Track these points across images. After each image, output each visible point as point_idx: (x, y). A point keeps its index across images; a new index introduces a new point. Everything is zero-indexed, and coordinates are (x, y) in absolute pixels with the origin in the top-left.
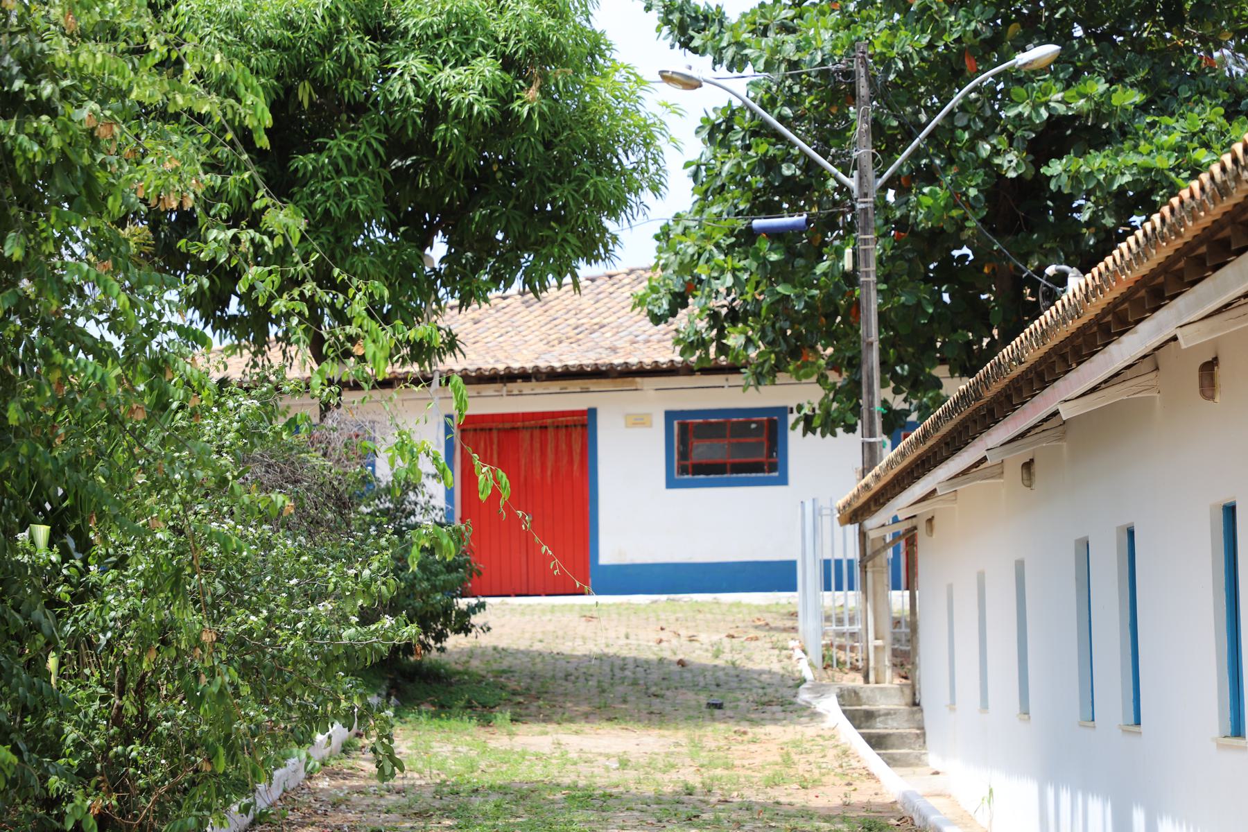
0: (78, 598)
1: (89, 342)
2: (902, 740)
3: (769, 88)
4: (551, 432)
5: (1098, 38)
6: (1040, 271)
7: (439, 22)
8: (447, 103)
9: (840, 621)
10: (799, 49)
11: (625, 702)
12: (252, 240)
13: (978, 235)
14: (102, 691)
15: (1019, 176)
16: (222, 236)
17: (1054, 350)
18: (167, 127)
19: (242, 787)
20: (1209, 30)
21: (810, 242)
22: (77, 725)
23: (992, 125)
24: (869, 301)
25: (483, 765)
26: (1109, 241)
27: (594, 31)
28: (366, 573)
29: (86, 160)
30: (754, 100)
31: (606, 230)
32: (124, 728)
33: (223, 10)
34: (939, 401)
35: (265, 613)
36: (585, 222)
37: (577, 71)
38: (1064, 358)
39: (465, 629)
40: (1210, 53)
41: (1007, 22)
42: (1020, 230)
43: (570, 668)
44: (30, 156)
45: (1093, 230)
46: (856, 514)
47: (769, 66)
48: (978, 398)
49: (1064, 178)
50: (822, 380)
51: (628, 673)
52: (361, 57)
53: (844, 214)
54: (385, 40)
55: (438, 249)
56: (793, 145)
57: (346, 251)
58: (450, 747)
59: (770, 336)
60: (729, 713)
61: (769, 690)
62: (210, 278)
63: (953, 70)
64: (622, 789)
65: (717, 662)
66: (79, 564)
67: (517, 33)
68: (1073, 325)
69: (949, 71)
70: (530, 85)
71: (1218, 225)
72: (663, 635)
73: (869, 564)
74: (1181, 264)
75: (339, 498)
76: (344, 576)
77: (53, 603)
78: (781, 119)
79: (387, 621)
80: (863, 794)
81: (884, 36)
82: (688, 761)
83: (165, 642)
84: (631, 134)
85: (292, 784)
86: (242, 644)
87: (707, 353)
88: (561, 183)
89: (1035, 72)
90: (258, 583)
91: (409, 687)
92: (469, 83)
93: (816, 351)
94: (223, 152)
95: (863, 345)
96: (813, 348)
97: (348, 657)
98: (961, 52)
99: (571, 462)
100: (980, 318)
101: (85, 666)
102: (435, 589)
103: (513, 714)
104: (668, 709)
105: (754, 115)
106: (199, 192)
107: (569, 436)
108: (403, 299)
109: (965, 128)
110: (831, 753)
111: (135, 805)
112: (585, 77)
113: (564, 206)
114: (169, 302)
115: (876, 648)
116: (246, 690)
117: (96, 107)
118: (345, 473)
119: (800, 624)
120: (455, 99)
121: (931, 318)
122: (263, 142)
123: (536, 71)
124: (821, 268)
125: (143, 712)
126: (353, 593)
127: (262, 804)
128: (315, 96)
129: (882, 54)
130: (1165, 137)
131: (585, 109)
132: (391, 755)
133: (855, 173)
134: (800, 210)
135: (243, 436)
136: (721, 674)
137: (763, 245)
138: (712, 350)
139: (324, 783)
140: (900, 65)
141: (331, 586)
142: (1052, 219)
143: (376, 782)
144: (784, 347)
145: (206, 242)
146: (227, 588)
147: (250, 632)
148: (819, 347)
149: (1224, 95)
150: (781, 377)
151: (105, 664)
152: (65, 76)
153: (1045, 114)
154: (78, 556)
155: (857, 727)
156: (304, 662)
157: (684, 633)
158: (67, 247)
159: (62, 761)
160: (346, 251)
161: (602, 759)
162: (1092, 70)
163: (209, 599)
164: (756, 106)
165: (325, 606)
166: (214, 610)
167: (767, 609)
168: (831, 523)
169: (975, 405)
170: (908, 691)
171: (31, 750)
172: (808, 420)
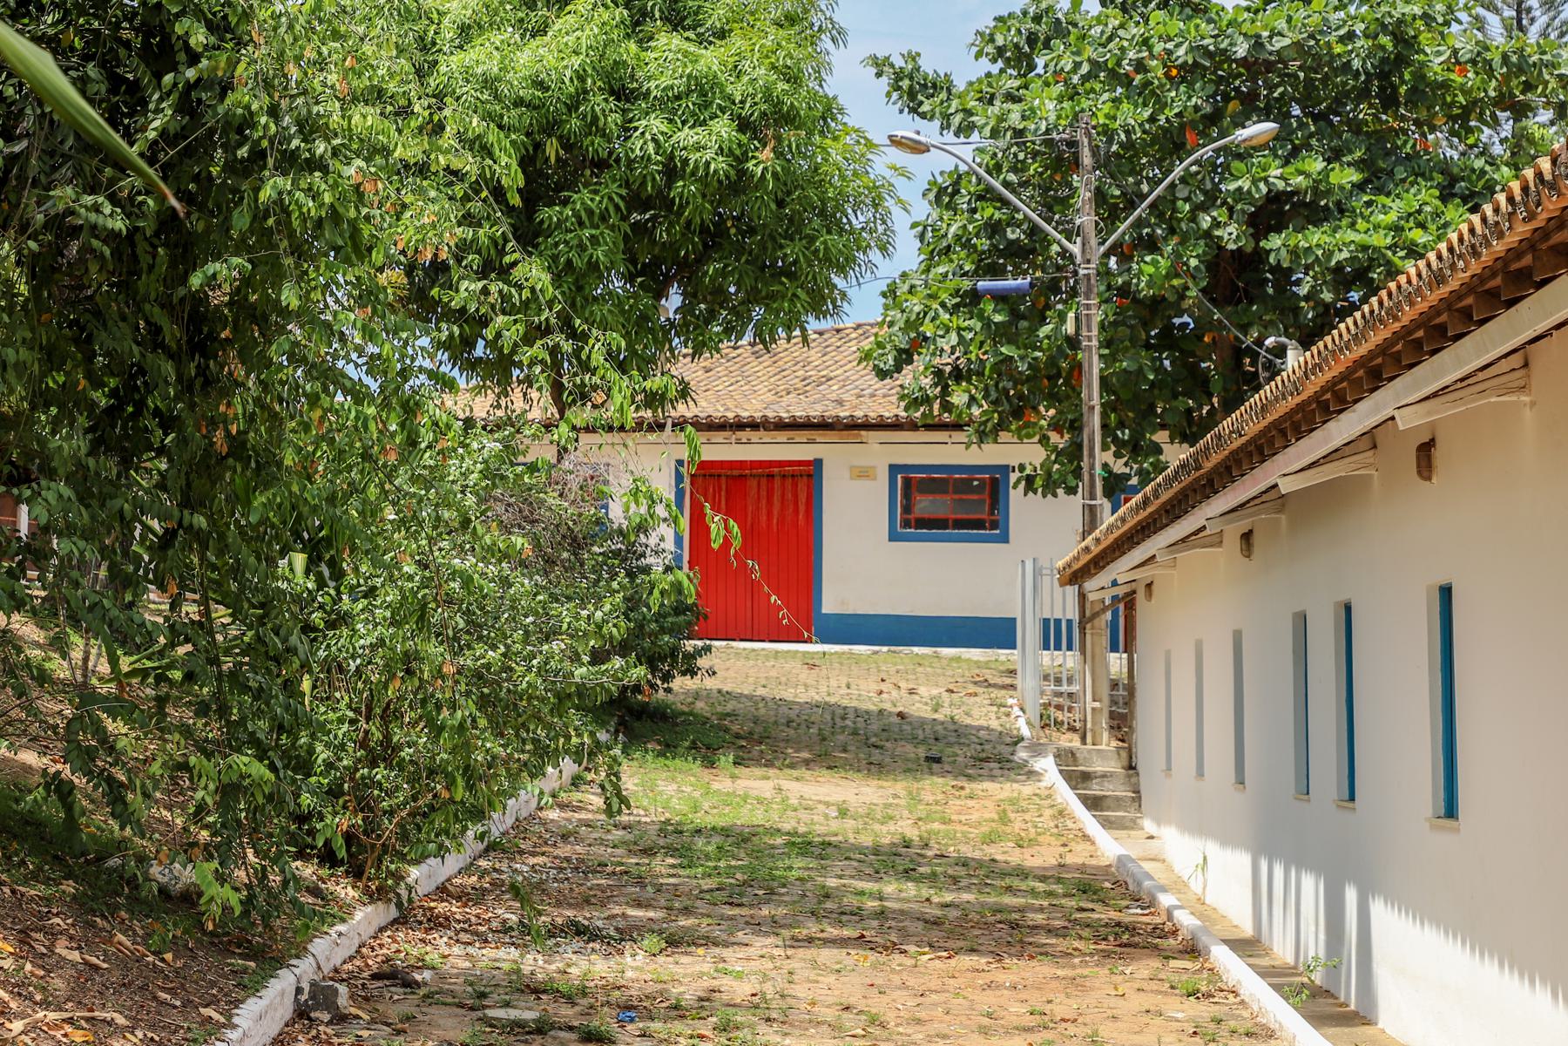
0: (331, 625)
1: (348, 384)
2: (1118, 802)
3: (995, 154)
4: (777, 482)
5: (1316, 118)
6: (1259, 342)
7: (680, 84)
8: (685, 162)
9: (1058, 681)
10: (1024, 118)
11: (845, 751)
12: (500, 291)
13: (1200, 305)
14: (351, 714)
15: (1239, 249)
16: (472, 287)
17: (1274, 424)
18: (425, 183)
19: (478, 814)
20: (1423, 115)
21: (1033, 304)
22: (327, 745)
23: (1211, 198)
24: (1091, 366)
25: (706, 806)
26: (1327, 318)
27: (826, 96)
28: (599, 614)
29: (352, 213)
30: (980, 165)
31: (835, 286)
32: (371, 751)
33: (479, 71)
34: (1159, 468)
35: (502, 649)
36: (814, 278)
37: (810, 134)
38: (1283, 433)
39: (691, 672)
40: (1423, 135)
41: (1227, 98)
42: (1240, 301)
43: (793, 715)
44: (305, 210)
45: (1312, 304)
46: (1076, 576)
47: (995, 134)
48: (1198, 468)
49: (1283, 252)
50: (1044, 441)
51: (848, 722)
52: (605, 117)
53: (1067, 279)
54: (628, 100)
56: (1018, 210)
57: (586, 300)
58: (675, 786)
59: (994, 395)
60: (947, 767)
61: (986, 747)
62: (460, 326)
63: (1174, 143)
64: (840, 838)
65: (936, 716)
66: (332, 592)
67: (754, 96)
68: (1292, 402)
69: (1171, 143)
70: (765, 146)
71: (1435, 311)
72: (883, 687)
73: (1088, 626)
74: (1399, 347)
75: (574, 539)
76: (577, 617)
77: (308, 628)
78: (1006, 184)
79: (617, 662)
80: (1078, 855)
81: (1106, 108)
82: (906, 813)
83: (409, 672)
84: (860, 194)
85: (524, 814)
86: (480, 677)
87: (931, 410)
88: (792, 240)
89: (1254, 148)
90: (497, 618)
91: (636, 724)
92: (708, 143)
93: (1038, 412)
94: (475, 206)
95: (1085, 409)
96: (1035, 409)
97: (580, 695)
98: (1182, 126)
99: (796, 511)
100: (1200, 385)
101: (336, 689)
102: (663, 630)
103: (736, 757)
104: (888, 760)
105: (979, 180)
106: (452, 244)
107: (795, 485)
108: (639, 347)
109: (1186, 200)
110: (1048, 813)
111: (379, 825)
112: (817, 139)
113: (795, 262)
114: (422, 349)
115: (1093, 709)
116: (483, 723)
117: (363, 164)
118: (580, 515)
119: (1018, 682)
120: (693, 157)
121: (1152, 384)
122: (515, 200)
123: (770, 133)
124: (1045, 330)
125: (387, 736)
126: (585, 634)
127: (495, 833)
128: (562, 152)
129: (1105, 125)
130: (1382, 216)
131: (816, 169)
132: (618, 794)
133: (1079, 240)
134: (1025, 273)
135: (486, 478)
136: (939, 728)
137: (988, 307)
138: (936, 406)
139: (554, 814)
140: (1123, 136)
141: (565, 626)
142: (1270, 291)
143: (603, 817)
144: (1006, 406)
145: (457, 291)
146: (467, 622)
147: (488, 666)
148: (1042, 408)
149: (1439, 178)
150: (1004, 436)
151: (355, 690)
152: (336, 135)
153: (1264, 189)
154: (332, 584)
155: (1074, 788)
156: (537, 698)
157: (903, 685)
158: (332, 294)
159: (313, 779)
160: (586, 300)
161: (821, 807)
162: (1309, 148)
163: (451, 633)
164: (981, 172)
165: (557, 646)
166: (456, 645)
167: (987, 665)
168: (1050, 583)
169: (1194, 475)
170: (1124, 754)
171: (286, 767)
172: (1030, 480)
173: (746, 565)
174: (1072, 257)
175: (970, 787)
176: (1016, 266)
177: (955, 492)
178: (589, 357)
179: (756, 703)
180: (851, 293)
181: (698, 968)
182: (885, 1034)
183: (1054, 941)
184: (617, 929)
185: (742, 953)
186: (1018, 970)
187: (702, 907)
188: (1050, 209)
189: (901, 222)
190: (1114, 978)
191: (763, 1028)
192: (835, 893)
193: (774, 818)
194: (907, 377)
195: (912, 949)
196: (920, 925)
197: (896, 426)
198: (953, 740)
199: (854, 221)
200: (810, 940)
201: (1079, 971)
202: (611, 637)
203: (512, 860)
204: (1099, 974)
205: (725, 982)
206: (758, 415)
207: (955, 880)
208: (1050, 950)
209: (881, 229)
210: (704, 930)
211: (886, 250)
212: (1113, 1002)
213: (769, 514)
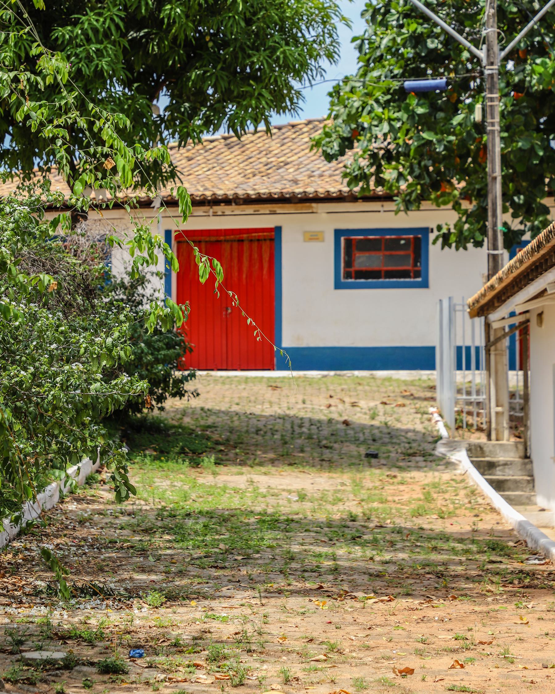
4: (246, 245)
9: (469, 393)
11: (302, 451)
12: (28, 80)
21: (448, 100)
24: (494, 146)
25: (194, 496)
28: (109, 340)
31: (292, 88)
36: (276, 81)
39: (180, 394)
43: (260, 425)
46: (482, 310)
50: (456, 206)
51: (304, 430)
55: (163, 101)
56: (436, 25)
58: (168, 482)
59: (417, 171)
60: (383, 461)
61: (414, 445)
64: (301, 516)
72: (332, 402)
73: (492, 348)
76: (92, 343)
79: (125, 378)
80: (487, 523)
82: (351, 496)
85: (48, 506)
87: (368, 185)
88: (258, 50)
93: (452, 185)
95: (489, 179)
102: (157, 361)
103: (217, 459)
104: (336, 457)
107: (260, 248)
110: (462, 493)
115: (497, 413)
119: (438, 395)
121: (542, 159)
124: (457, 120)
126: (98, 357)
133: (484, 47)
134: (442, 74)
135: (16, 234)
136: (376, 431)
137: (413, 101)
139: (72, 506)
144: (427, 180)
150: (425, 205)
155: (483, 474)
157: (347, 400)
161: (285, 494)
170: (521, 447)
173: (228, 295)
174: (479, 61)
175: (400, 476)
176: (435, 70)
177: (386, 249)
178: (101, 129)
179: (231, 417)
180: (304, 92)
181: (192, 616)
182: (342, 658)
183: (471, 586)
184: (126, 589)
185: (226, 603)
186: (443, 608)
187: (194, 571)
188: (462, 23)
189: (344, 35)
190: (519, 611)
191: (245, 657)
192: (298, 556)
193: (248, 503)
194: (348, 158)
195: (360, 595)
196: (366, 577)
197: (340, 198)
198: (387, 440)
199: (307, 36)
200: (280, 592)
201: (492, 607)
202: (120, 358)
203: (41, 541)
204: (508, 610)
205: (214, 625)
206: (230, 193)
207: (392, 544)
208: (468, 593)
209: (328, 41)
210: (196, 587)
211: (333, 57)
212: (519, 628)
213: (240, 271)
